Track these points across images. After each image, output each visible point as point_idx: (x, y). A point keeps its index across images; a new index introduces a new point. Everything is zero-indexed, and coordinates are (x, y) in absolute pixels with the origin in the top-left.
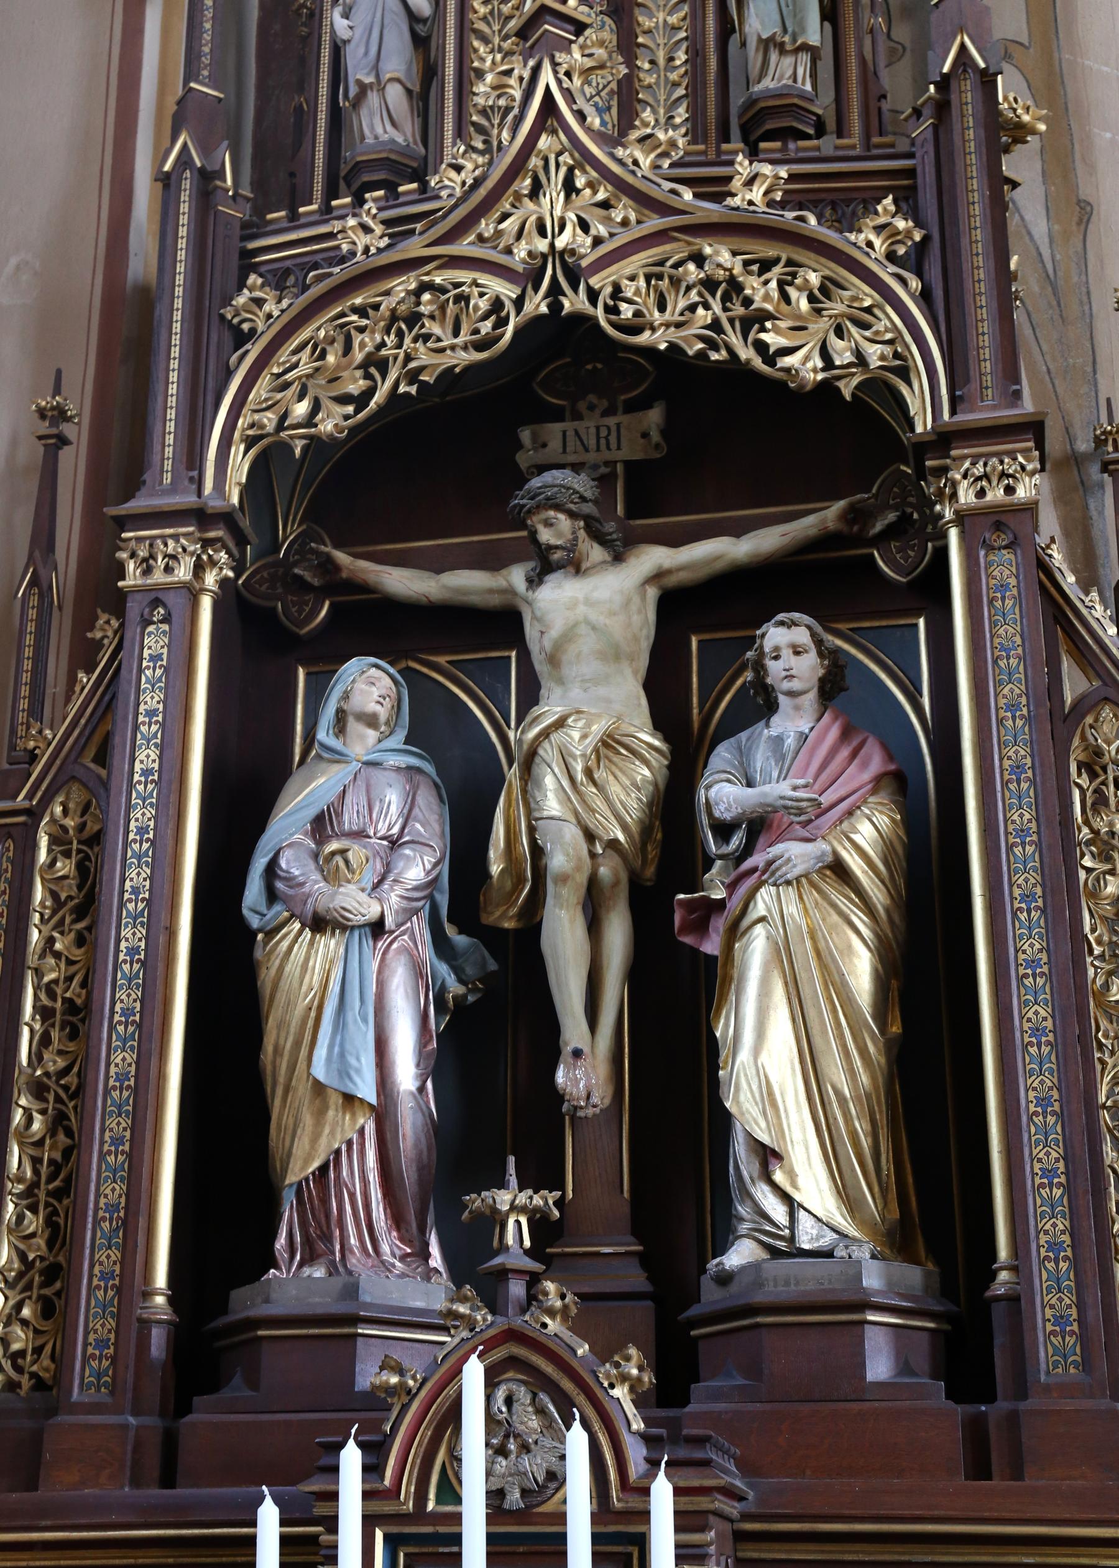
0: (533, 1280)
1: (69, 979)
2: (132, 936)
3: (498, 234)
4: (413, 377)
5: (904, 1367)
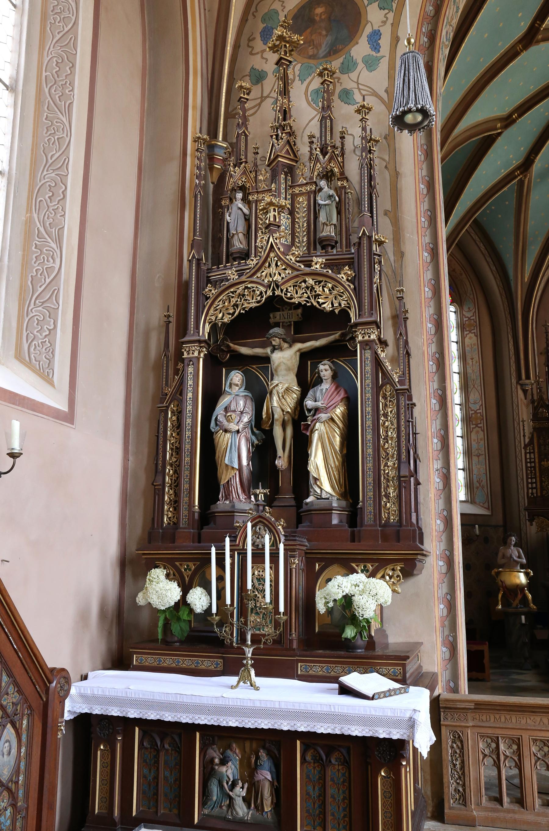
0: (264, 506)
1: (176, 442)
2: (188, 434)
3: (261, 276)
4: (244, 309)
5: (341, 521)
